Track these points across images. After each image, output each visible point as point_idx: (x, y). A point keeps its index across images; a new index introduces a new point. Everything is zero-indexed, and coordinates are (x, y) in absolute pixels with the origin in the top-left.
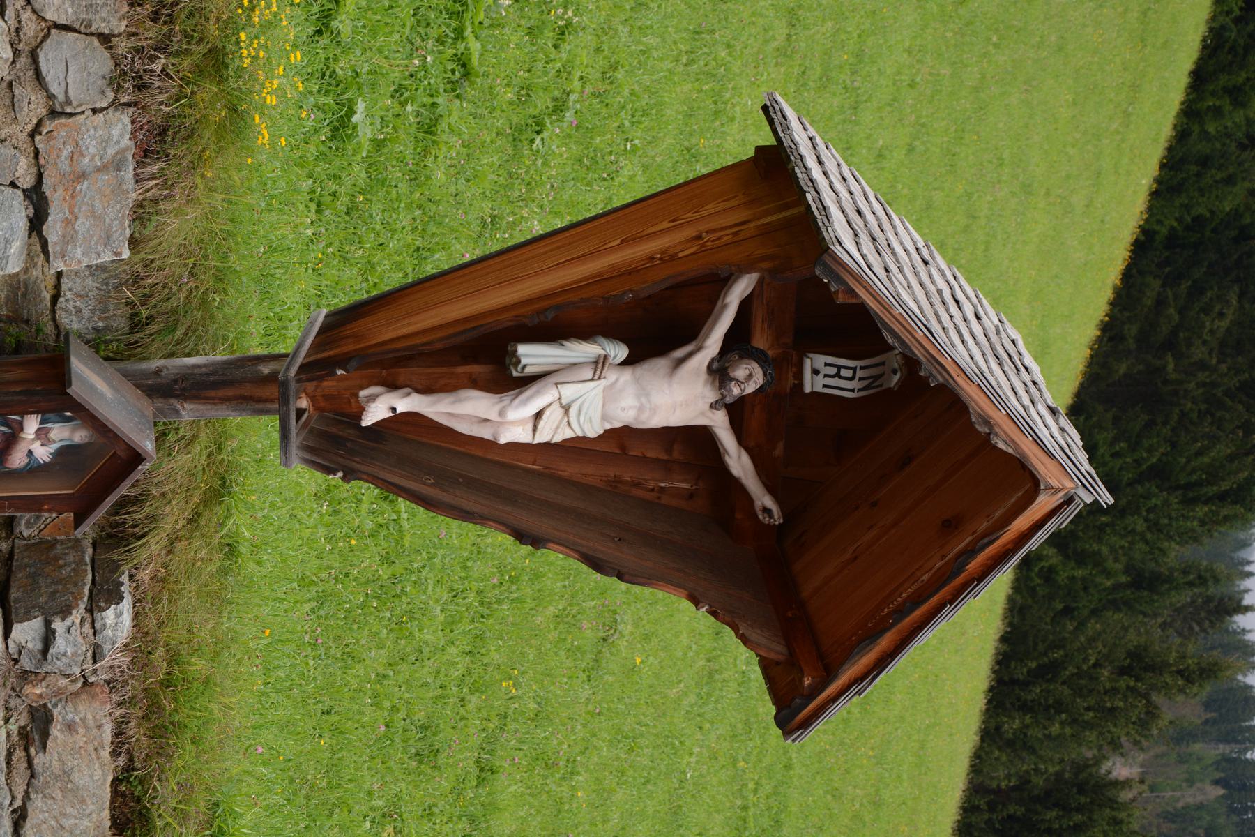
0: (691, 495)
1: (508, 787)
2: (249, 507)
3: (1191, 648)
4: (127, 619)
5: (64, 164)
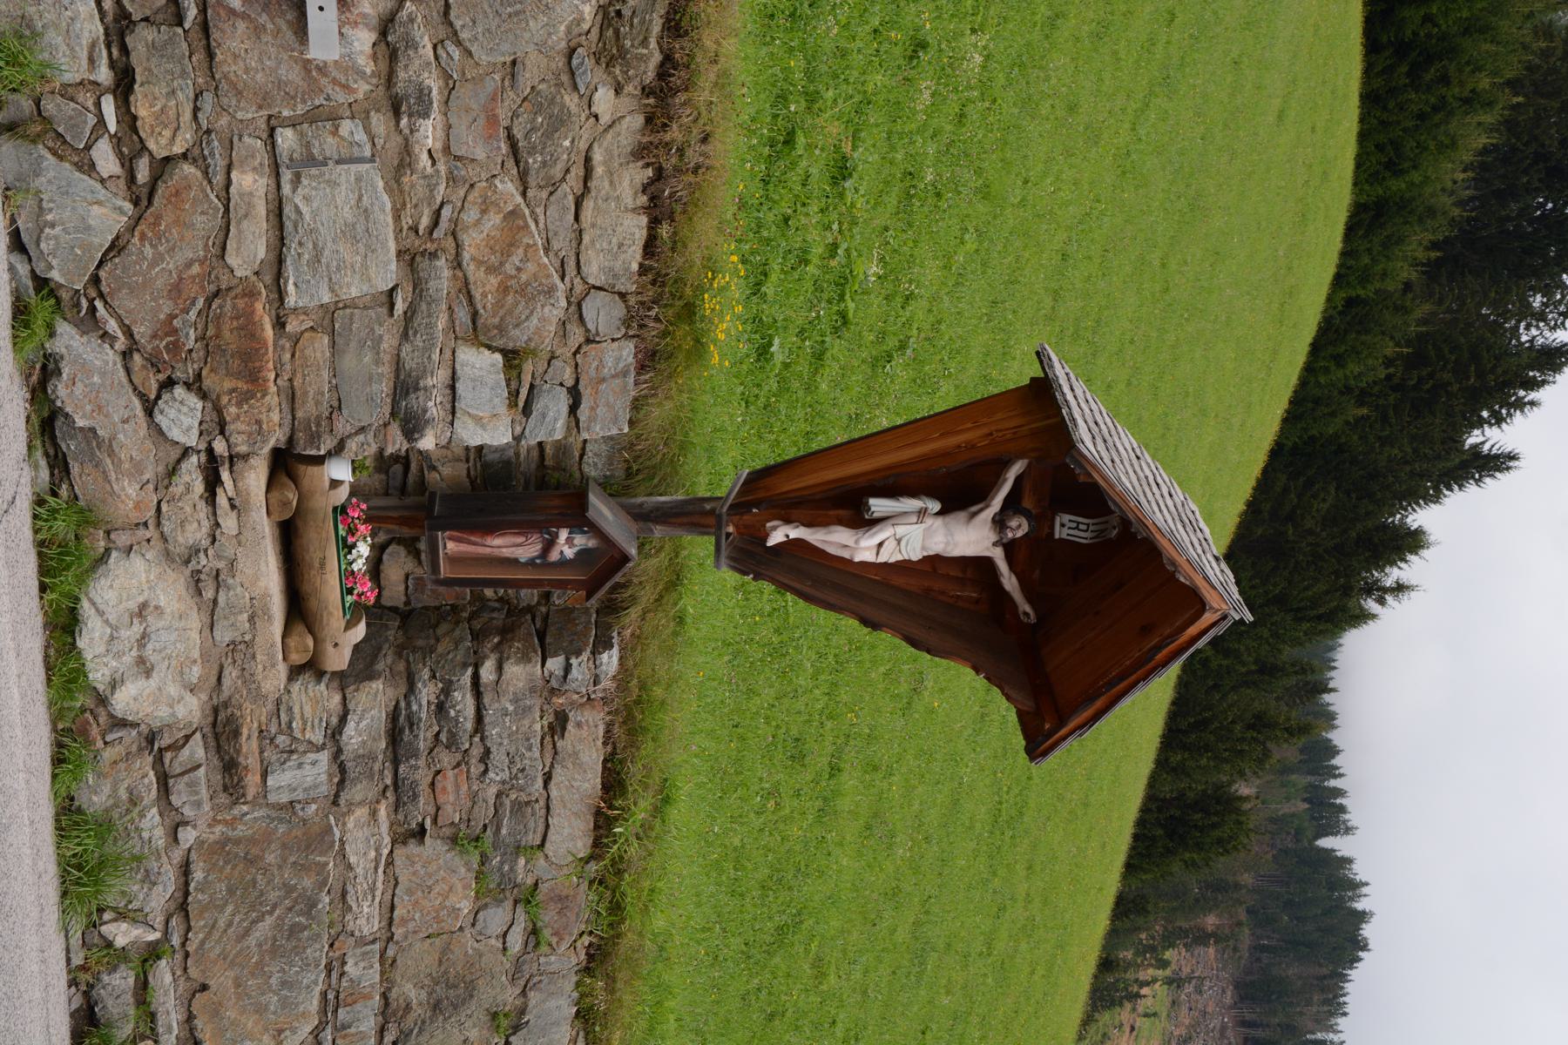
0: (977, 601)
1: (849, 781)
2: (693, 593)
3: (1294, 714)
4: (615, 660)
5: (592, 373)
